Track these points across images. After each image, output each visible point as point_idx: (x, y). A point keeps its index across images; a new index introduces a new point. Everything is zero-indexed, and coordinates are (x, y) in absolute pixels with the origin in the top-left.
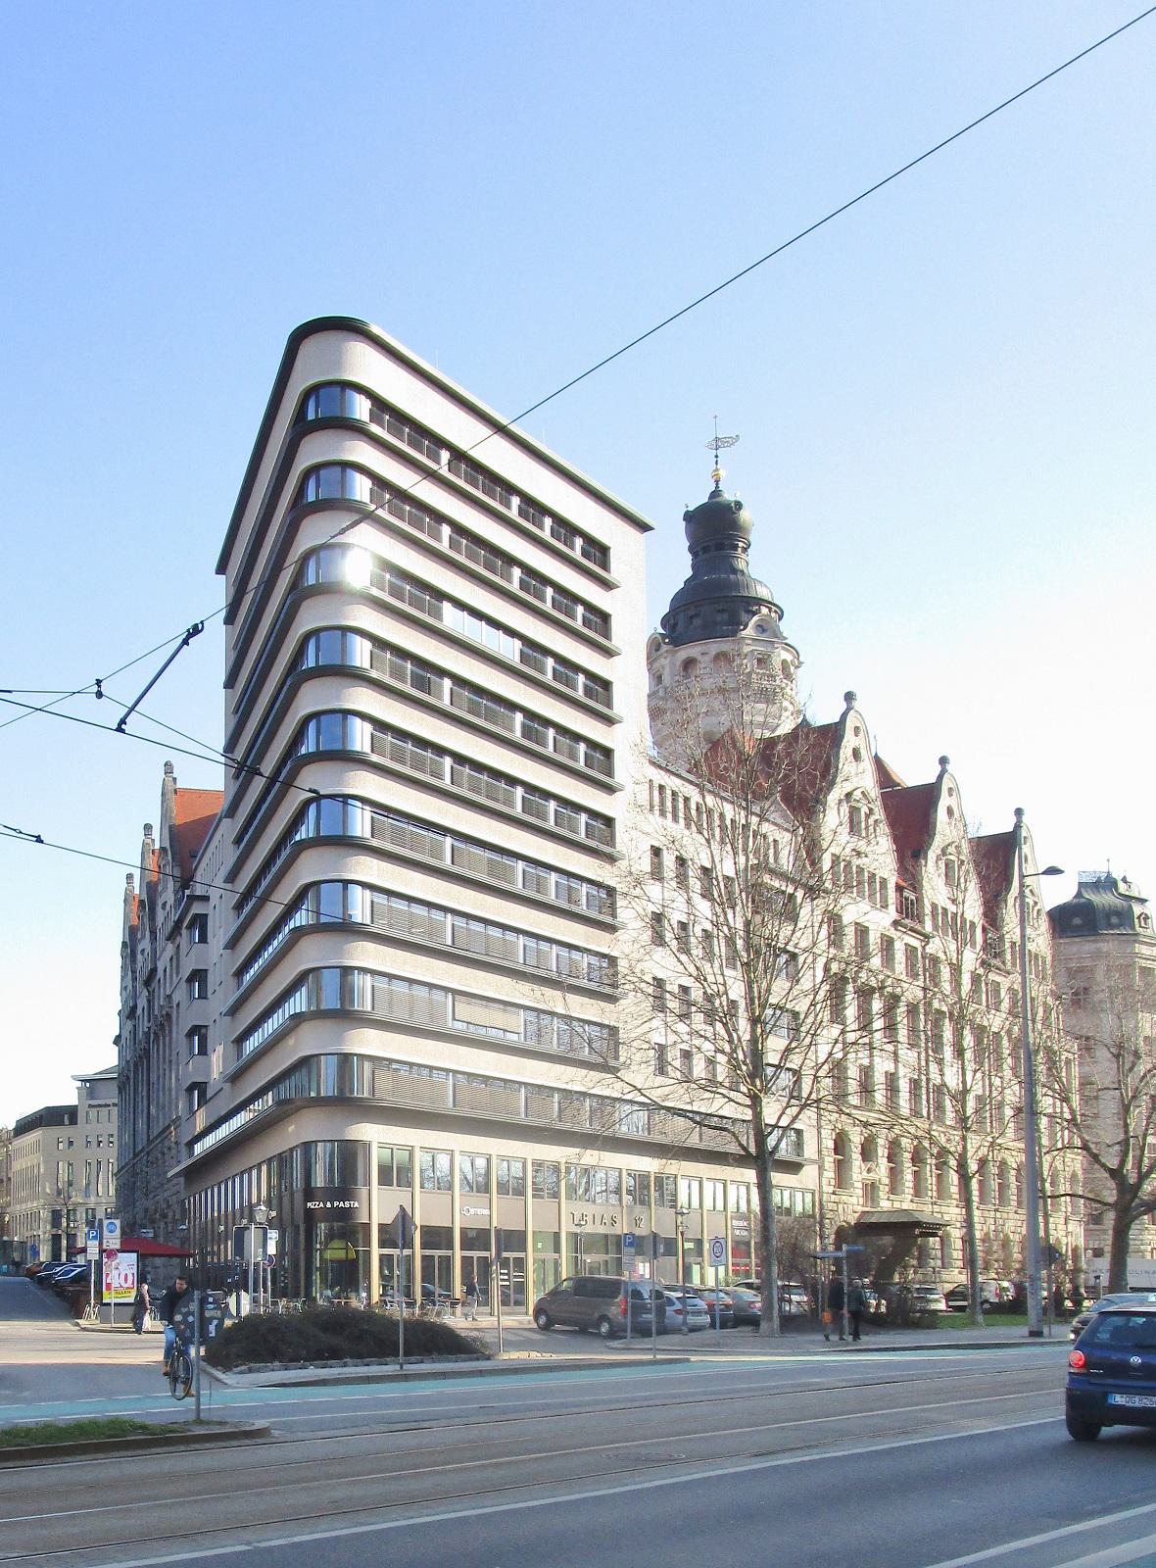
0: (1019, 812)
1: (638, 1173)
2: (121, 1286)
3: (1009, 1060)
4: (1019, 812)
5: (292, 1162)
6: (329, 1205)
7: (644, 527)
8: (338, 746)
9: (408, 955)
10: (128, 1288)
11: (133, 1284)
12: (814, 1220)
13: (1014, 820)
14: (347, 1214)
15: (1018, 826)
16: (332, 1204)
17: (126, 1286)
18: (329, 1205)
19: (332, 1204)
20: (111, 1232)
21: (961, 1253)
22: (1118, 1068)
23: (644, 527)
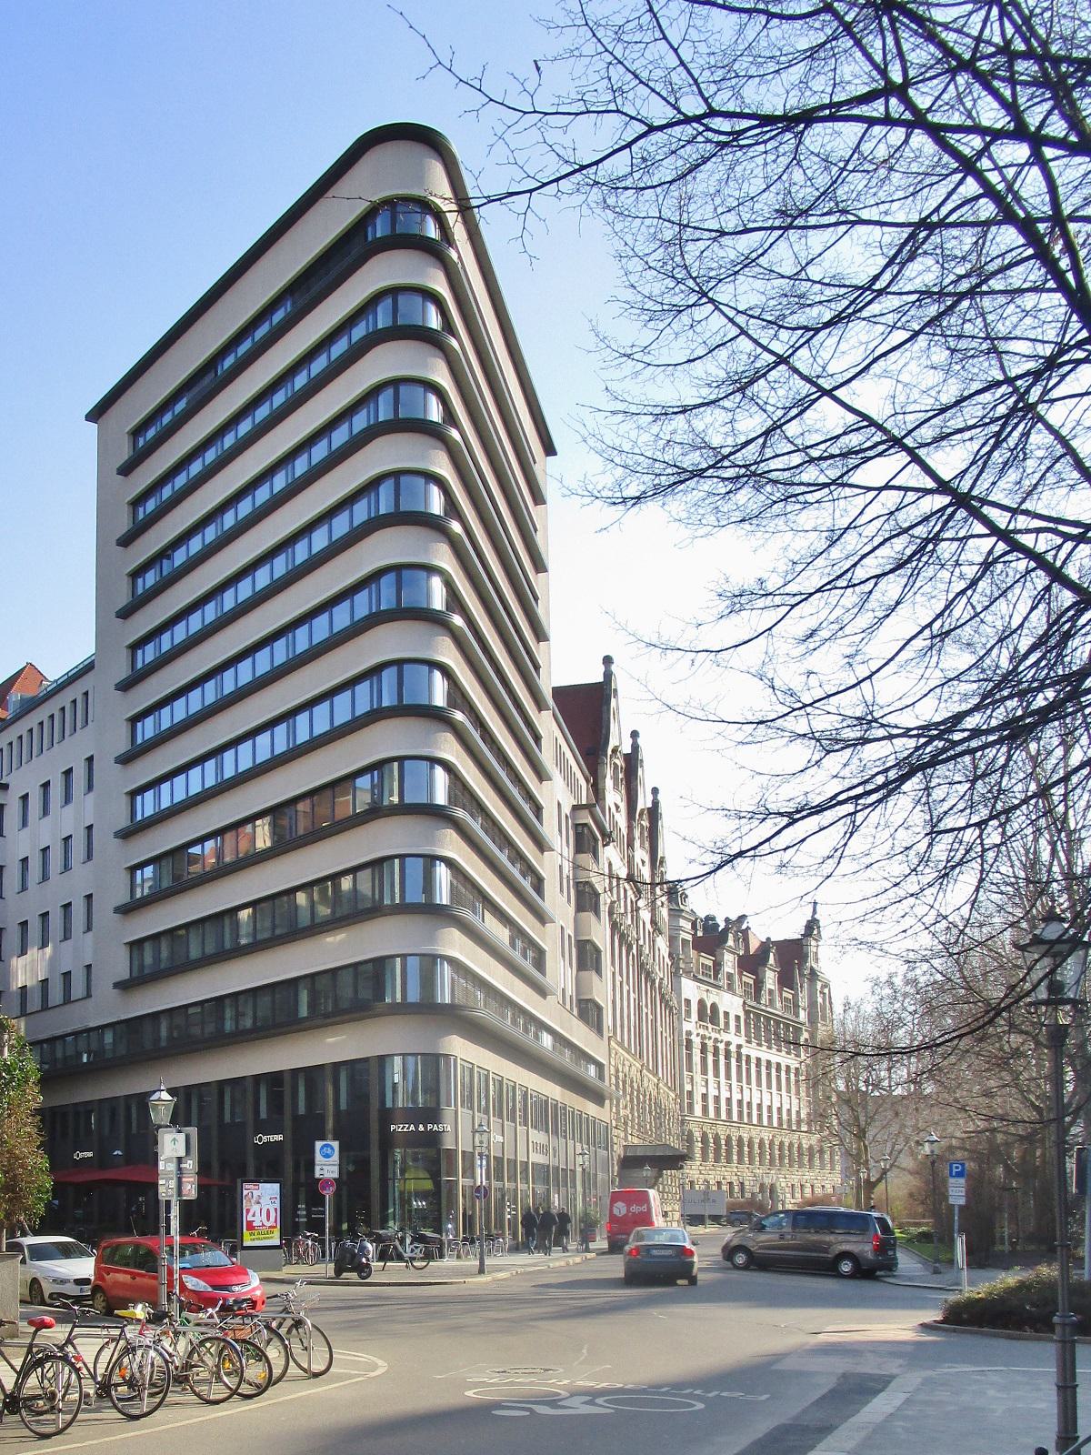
0: (608, 661)
1: (534, 1094)
2: (263, 1225)
3: (700, 1145)
4: (608, 661)
5: (463, 1096)
6: (421, 1128)
7: (559, 804)
8: (422, 799)
9: (529, 991)
10: (270, 1227)
11: (276, 1221)
12: (48, 1205)
13: (602, 669)
14: (433, 1139)
15: (608, 675)
16: (426, 1127)
17: (268, 1224)
18: (421, 1128)
19: (426, 1127)
20: (327, 1156)
21: (1064, 434)
22: (762, 255)
23: (559, 804)
